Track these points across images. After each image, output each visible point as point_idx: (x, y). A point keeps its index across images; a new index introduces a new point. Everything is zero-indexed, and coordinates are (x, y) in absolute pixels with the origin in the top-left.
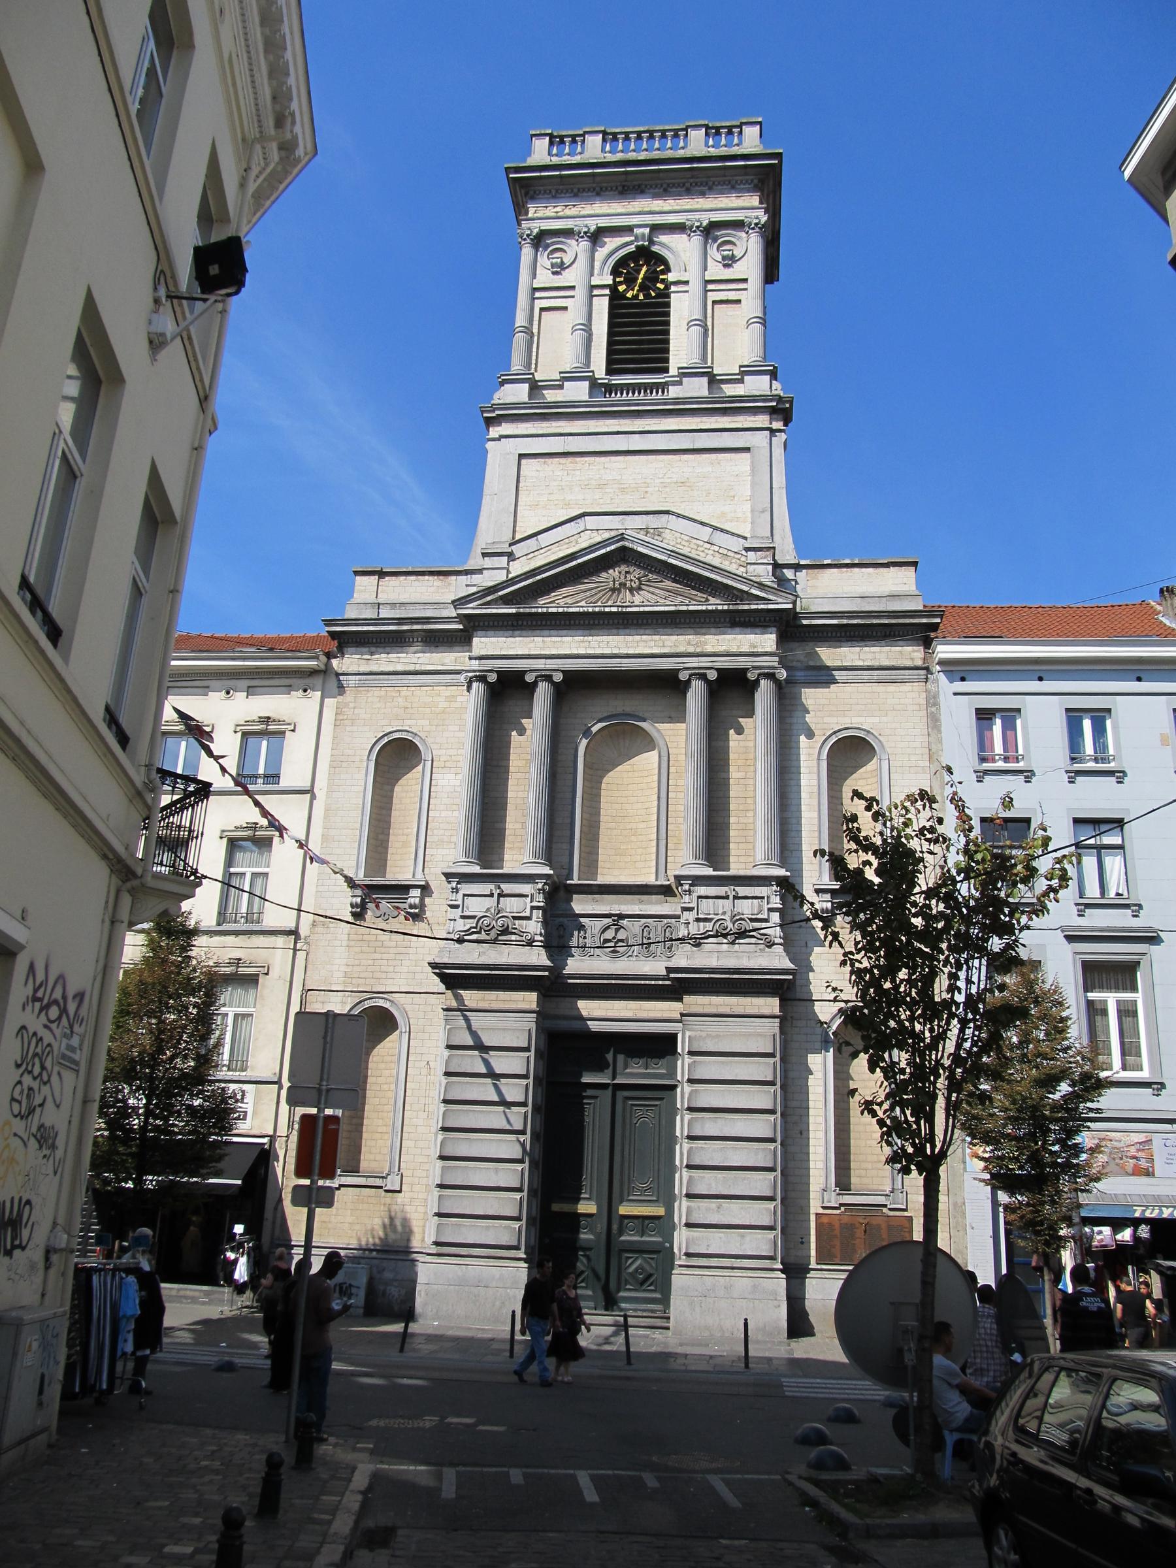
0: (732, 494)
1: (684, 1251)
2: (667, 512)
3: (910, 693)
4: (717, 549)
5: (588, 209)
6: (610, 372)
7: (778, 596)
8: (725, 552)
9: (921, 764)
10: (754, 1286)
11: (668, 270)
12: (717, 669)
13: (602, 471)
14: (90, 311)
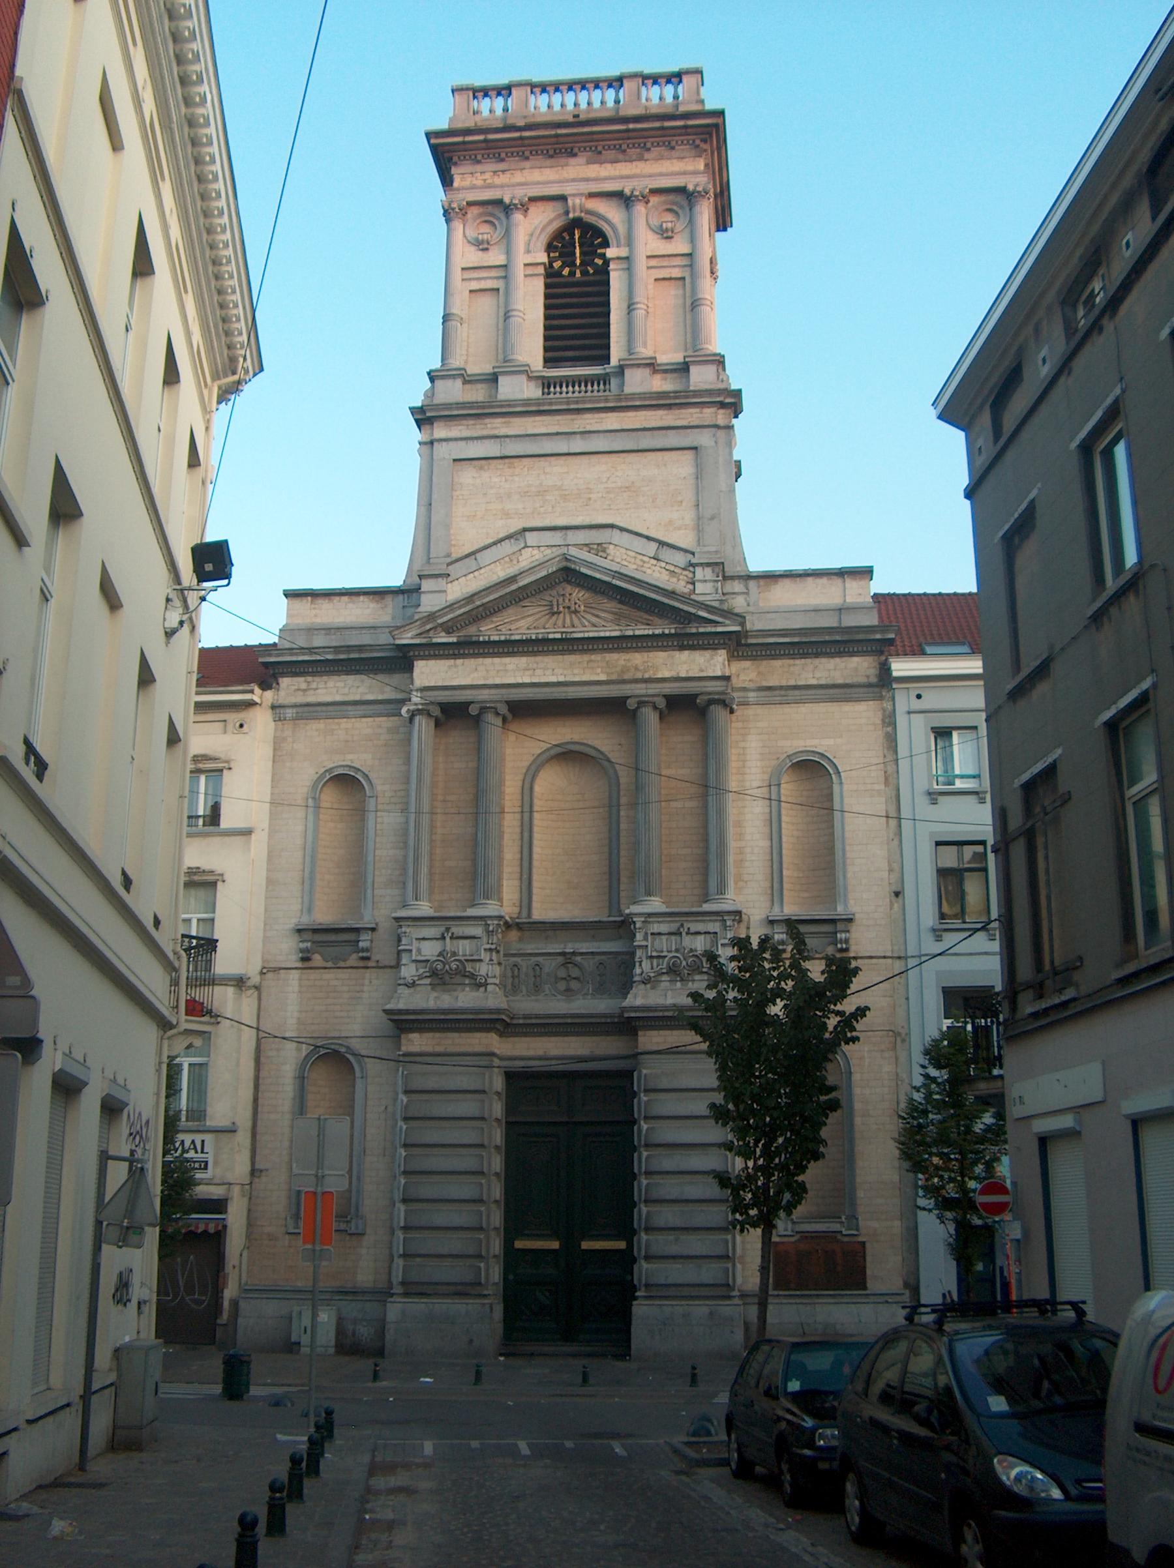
0: (680, 498)
1: (644, 1282)
2: (612, 526)
3: (862, 714)
4: (663, 565)
5: (518, 177)
6: (548, 361)
7: (725, 618)
8: (672, 568)
9: (876, 787)
10: (711, 1314)
11: (606, 244)
12: (665, 696)
13: (542, 477)
14: (58, 461)
